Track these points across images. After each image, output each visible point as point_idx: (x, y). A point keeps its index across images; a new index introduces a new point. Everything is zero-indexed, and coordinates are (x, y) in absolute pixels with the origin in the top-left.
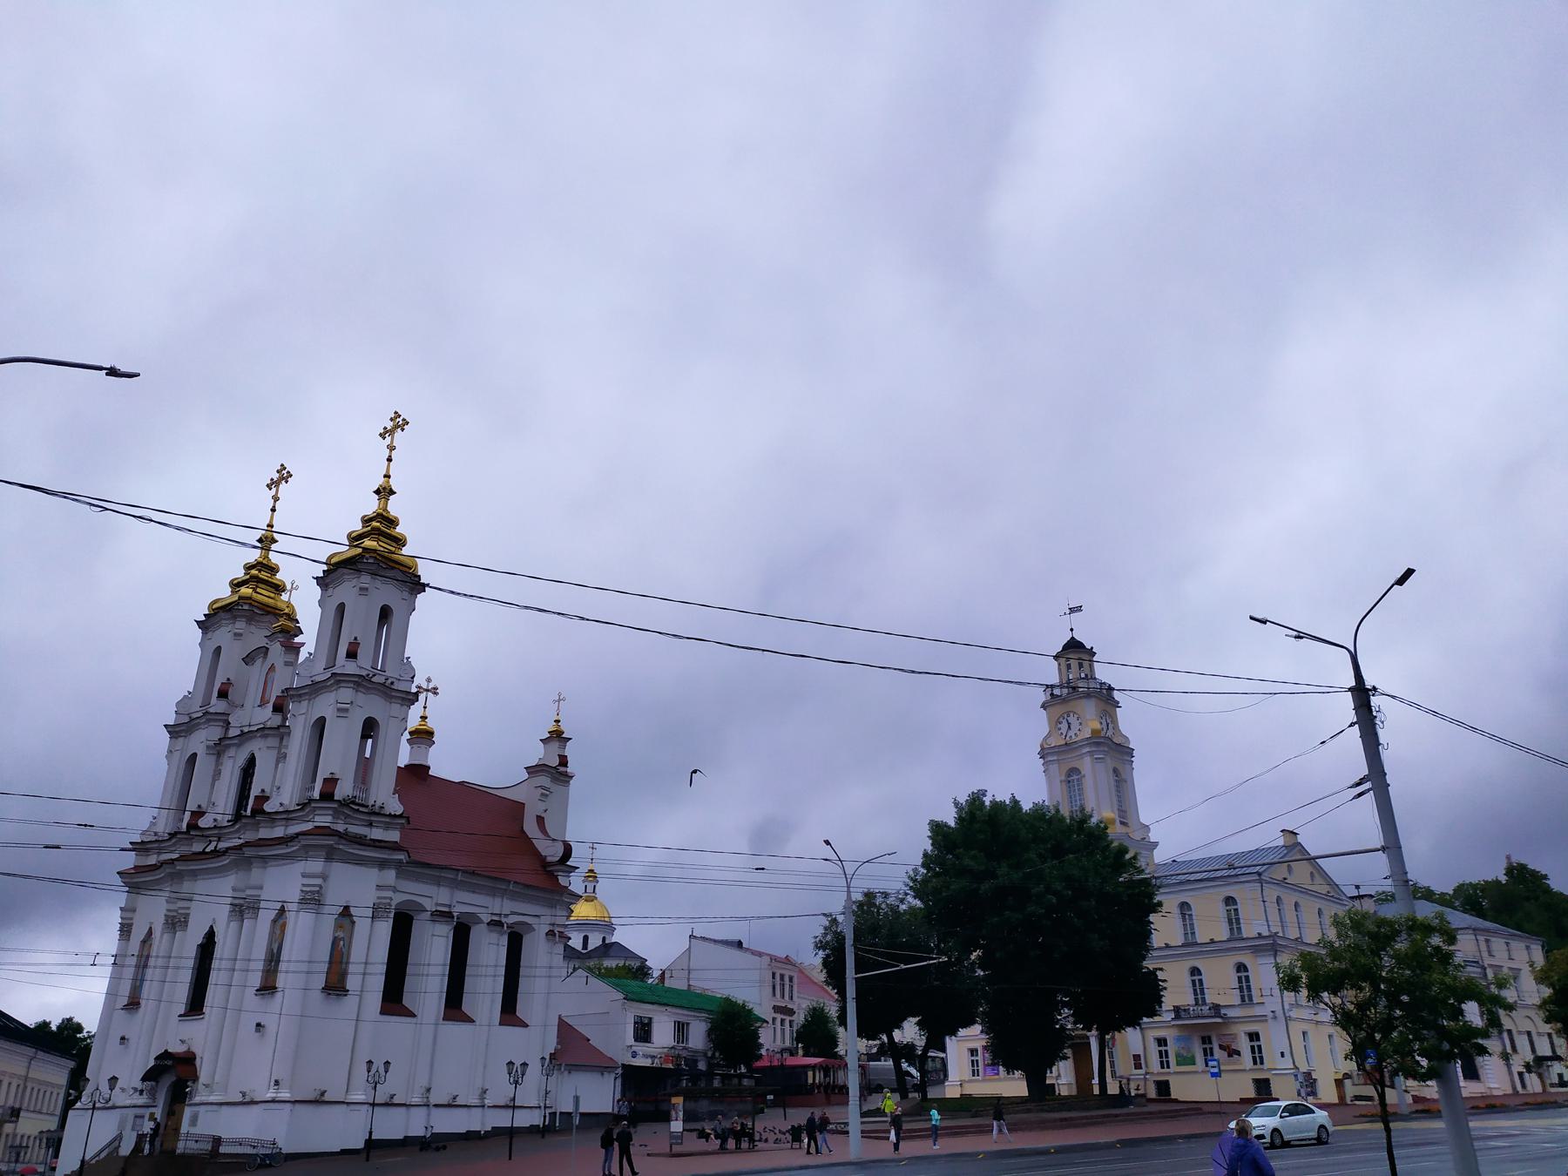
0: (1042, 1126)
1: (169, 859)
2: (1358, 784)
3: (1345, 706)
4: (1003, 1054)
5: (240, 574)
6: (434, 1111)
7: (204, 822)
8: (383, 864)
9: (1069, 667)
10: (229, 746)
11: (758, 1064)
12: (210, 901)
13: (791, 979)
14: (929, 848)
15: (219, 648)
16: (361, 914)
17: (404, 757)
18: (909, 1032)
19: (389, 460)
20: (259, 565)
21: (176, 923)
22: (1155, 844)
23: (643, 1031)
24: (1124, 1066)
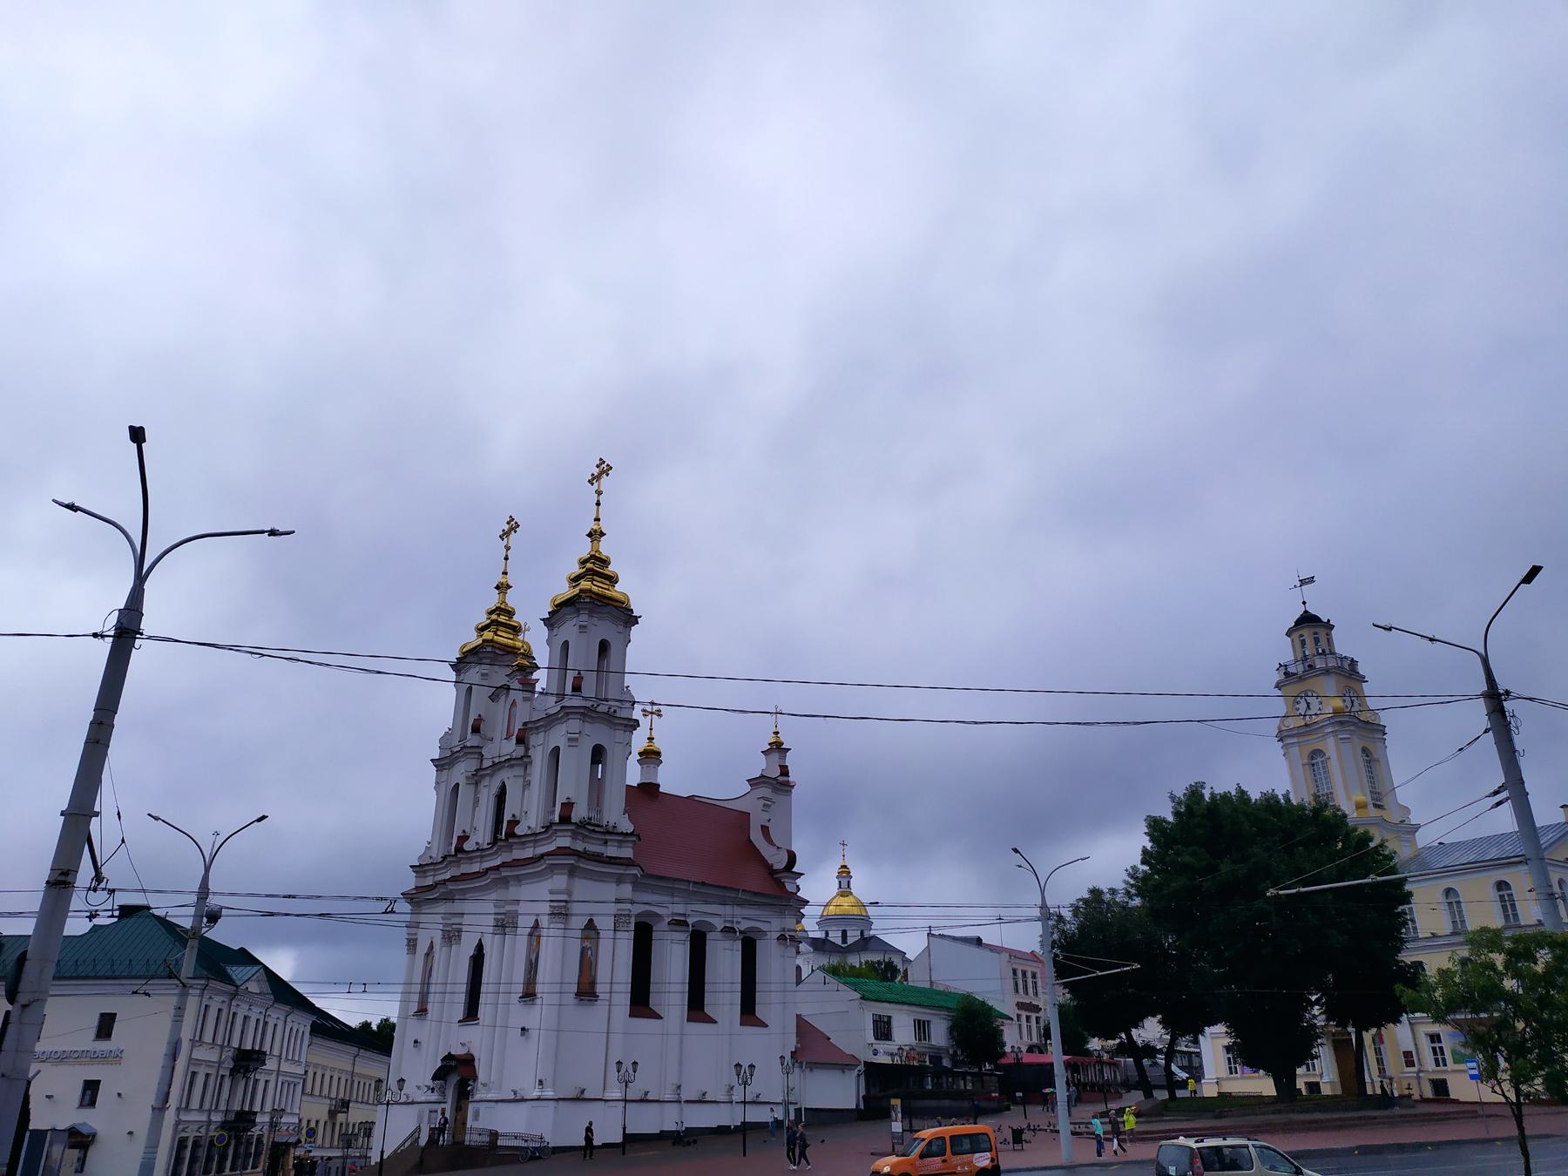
0: (1288, 1128)
1: (442, 880)
2: (1496, 793)
3: (1478, 715)
4: (1245, 1054)
5: (483, 619)
6: (685, 1106)
7: (468, 846)
8: (619, 880)
9: (1303, 643)
10: (483, 776)
11: (1003, 1061)
12: (478, 915)
13: (1034, 976)
14: (1149, 845)
15: (566, 643)
16: (605, 924)
17: (634, 774)
18: (1151, 1031)
19: (598, 504)
20: (499, 610)
21: (452, 936)
22: (1417, 827)
23: (883, 1029)
24: (1394, 1065)
